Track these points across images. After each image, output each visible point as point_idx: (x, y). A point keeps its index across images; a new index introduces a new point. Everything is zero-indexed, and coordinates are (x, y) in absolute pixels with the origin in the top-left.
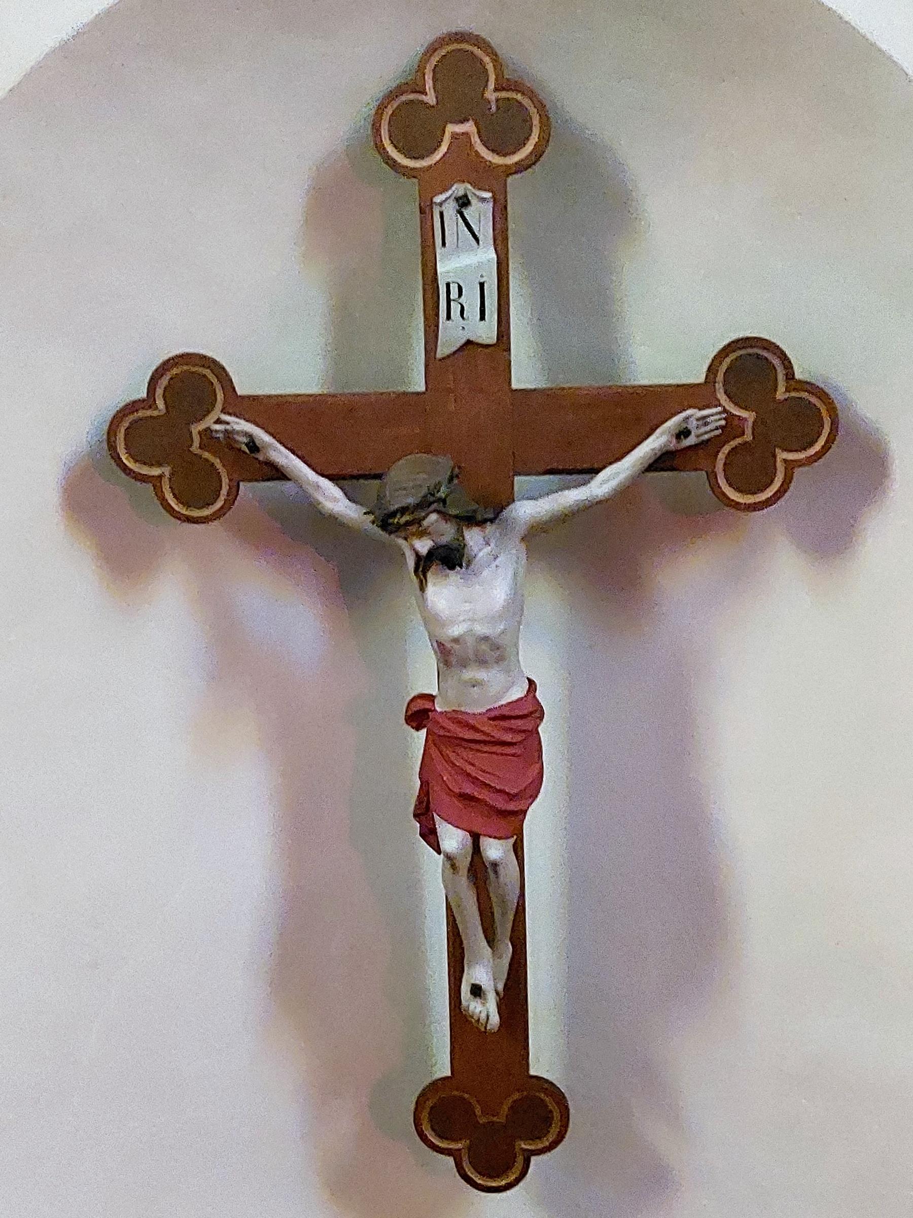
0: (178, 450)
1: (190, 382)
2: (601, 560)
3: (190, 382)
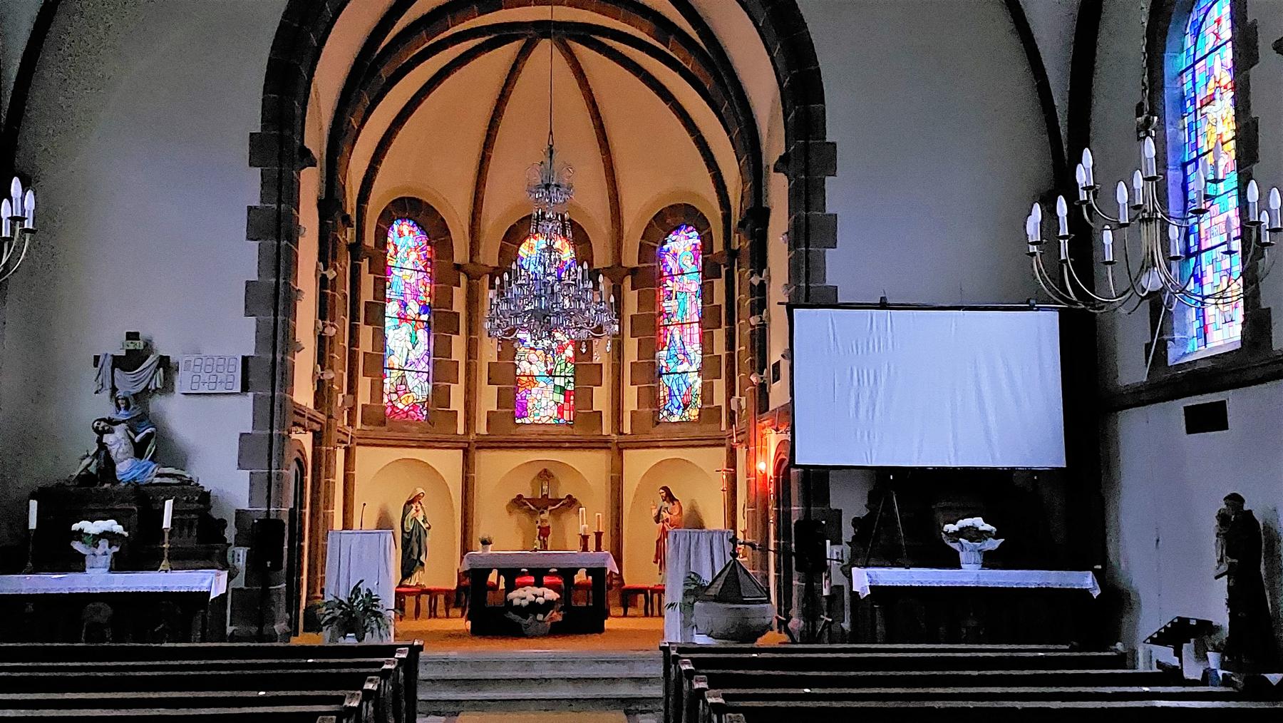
0: (518, 502)
1: (520, 497)
2: (556, 514)
3: (520, 497)
